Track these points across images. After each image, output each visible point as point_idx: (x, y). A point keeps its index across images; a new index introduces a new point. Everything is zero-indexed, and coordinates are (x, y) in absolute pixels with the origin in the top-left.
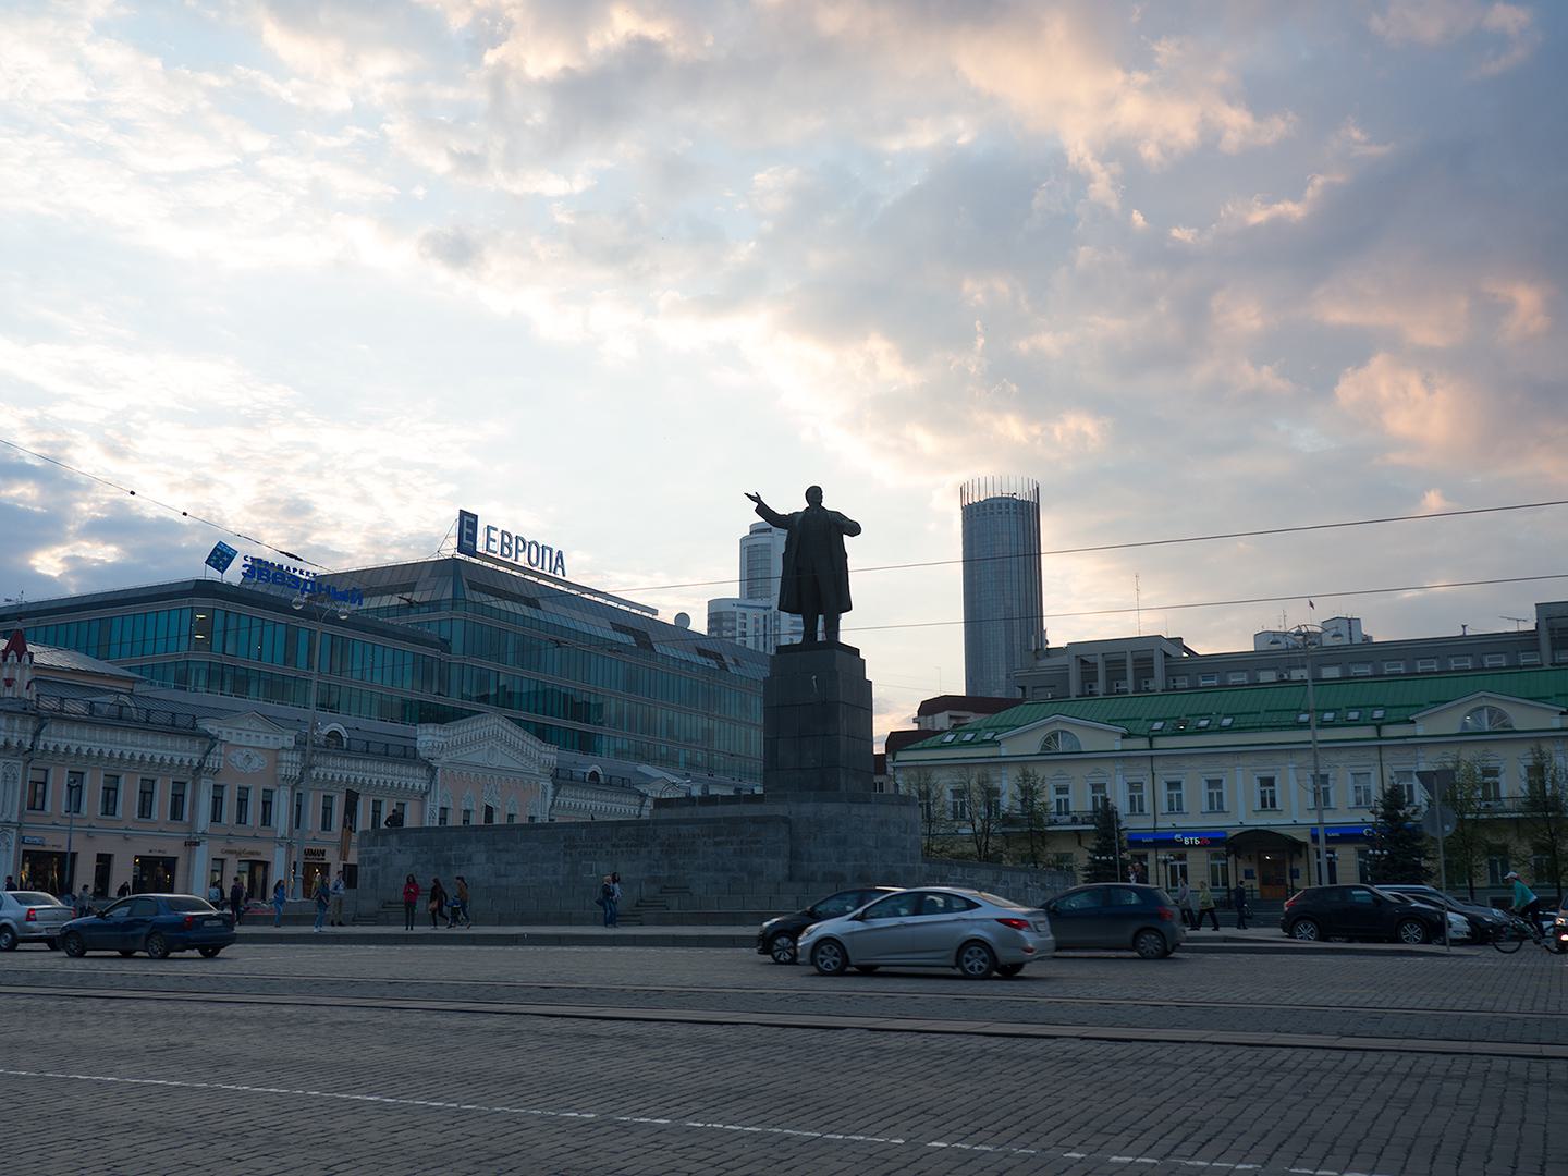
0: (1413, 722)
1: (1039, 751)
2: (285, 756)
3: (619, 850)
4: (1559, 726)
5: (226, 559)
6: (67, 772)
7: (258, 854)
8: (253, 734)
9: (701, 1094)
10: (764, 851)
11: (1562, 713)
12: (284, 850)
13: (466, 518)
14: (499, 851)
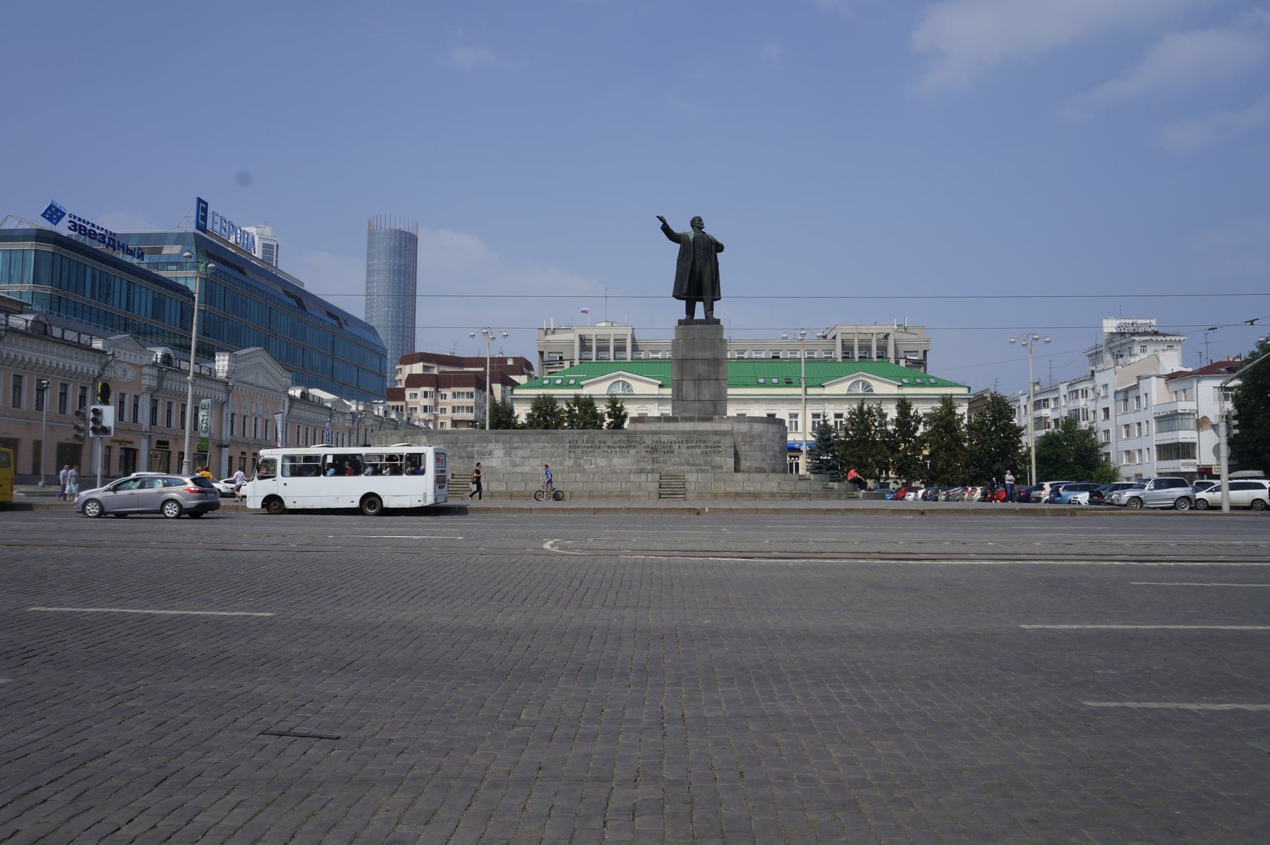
0: (823, 386)
2: (146, 370)
3: (613, 450)
4: (896, 393)
5: (59, 214)
6: (12, 376)
7: (132, 443)
8: (128, 353)
9: (405, 587)
10: (724, 453)
11: (899, 386)
12: (147, 440)
13: (201, 204)
14: (515, 448)
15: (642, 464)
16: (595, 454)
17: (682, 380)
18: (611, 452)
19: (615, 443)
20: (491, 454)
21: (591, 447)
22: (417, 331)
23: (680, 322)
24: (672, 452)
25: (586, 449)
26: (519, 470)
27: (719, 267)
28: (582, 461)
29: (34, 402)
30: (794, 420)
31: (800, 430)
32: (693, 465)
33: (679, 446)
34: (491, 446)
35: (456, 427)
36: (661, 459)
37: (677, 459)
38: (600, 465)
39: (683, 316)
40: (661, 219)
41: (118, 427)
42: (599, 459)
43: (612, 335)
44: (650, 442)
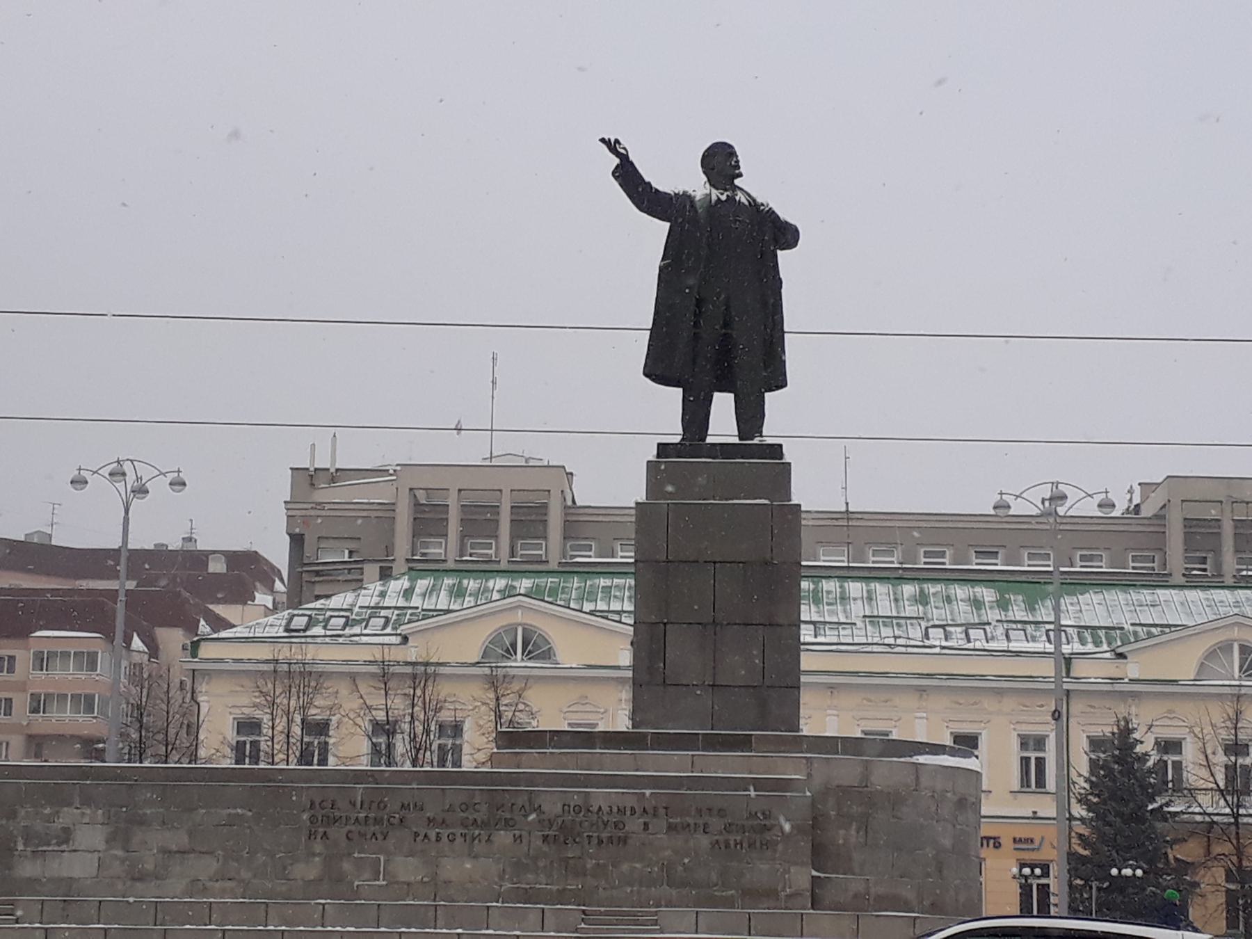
1: (1192, 678)
3: (445, 833)
15: (530, 876)
16: (391, 841)
18: (438, 839)
20: (66, 841)
25: (363, 829)
26: (148, 894)
28: (347, 866)
30: (1033, 755)
31: (1051, 784)
32: (684, 884)
33: (646, 824)
34: (67, 816)
35: (37, 756)
36: (590, 864)
39: (673, 431)
40: (612, 146)
42: (399, 859)
43: (506, 492)
44: (558, 809)
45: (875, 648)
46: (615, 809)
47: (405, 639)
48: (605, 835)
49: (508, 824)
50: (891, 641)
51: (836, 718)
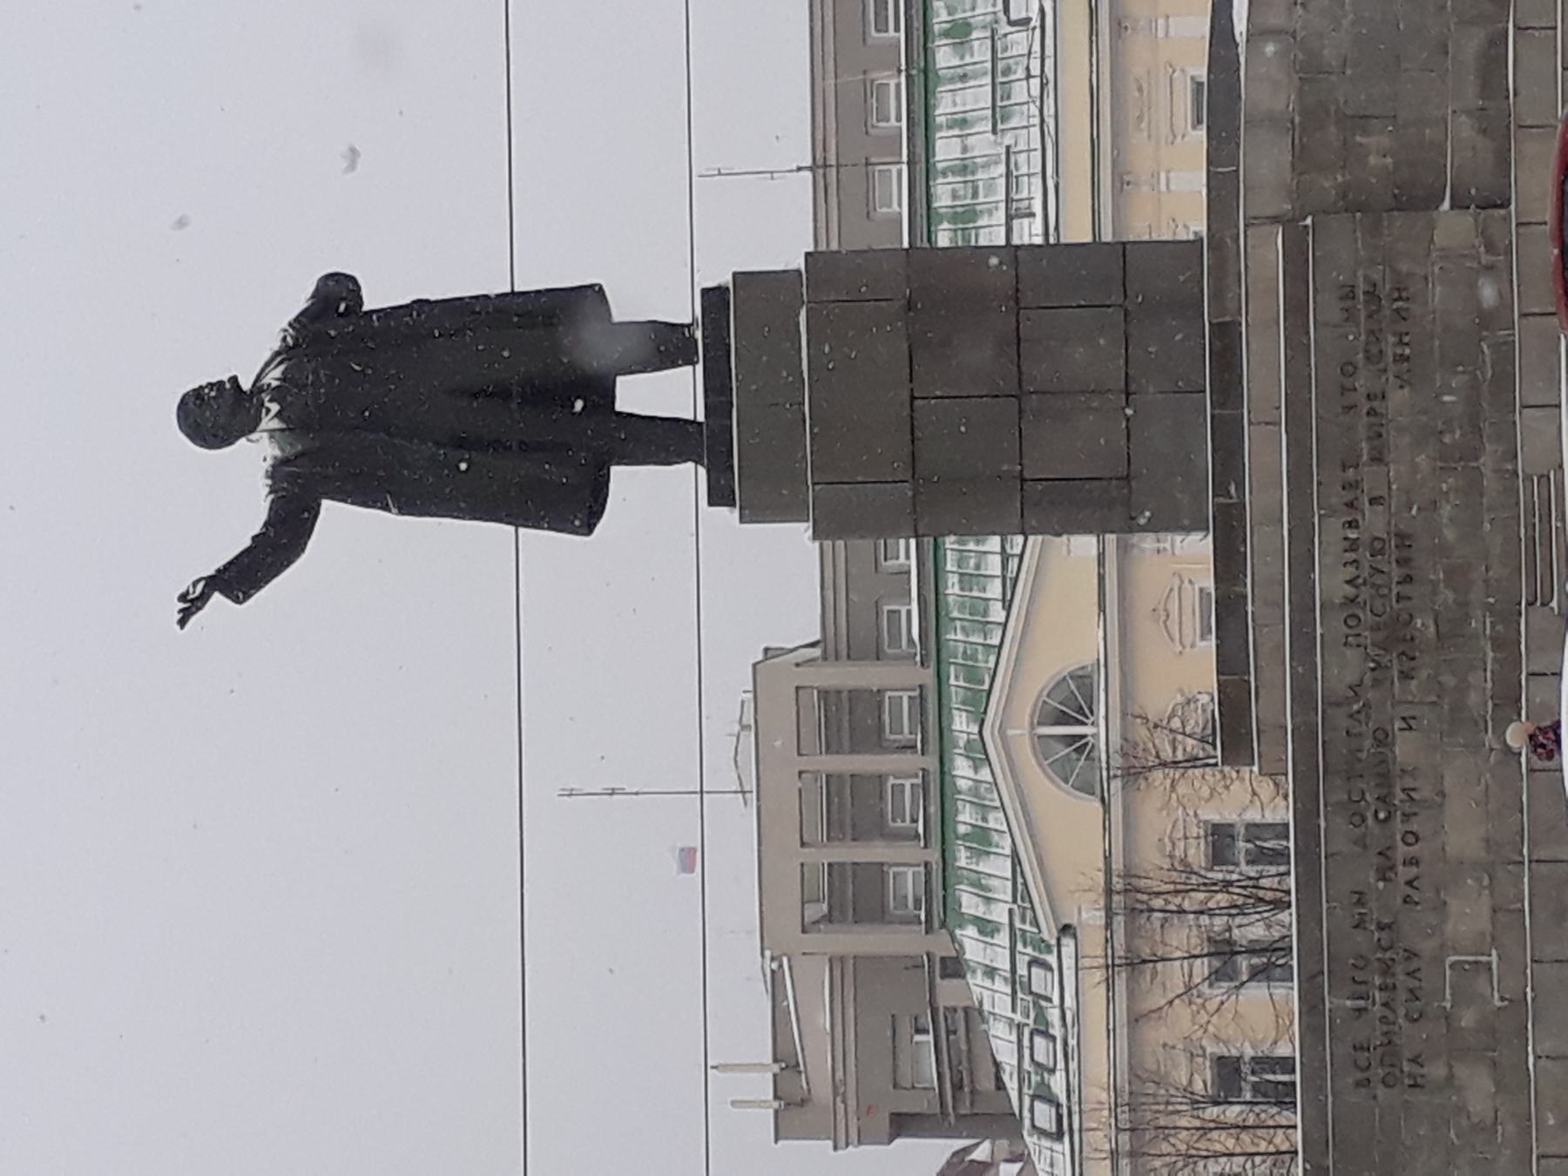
3: (1402, 851)
15: (1473, 698)
16: (1427, 947)
17: (1023, 480)
18: (1413, 861)
19: (1361, 842)
21: (1387, 969)
22: (527, 282)
23: (719, 495)
24: (1404, 540)
25: (1402, 995)
27: (433, 298)
28: (1468, 1019)
29: (1121, 848)
33: (1373, 501)
37: (1446, 510)
38: (1483, 922)
39: (688, 478)
40: (191, 605)
41: (1557, 774)
45: (1049, 110)
46: (1350, 556)
47: (1066, 929)
48: (1396, 573)
49: (1383, 739)
50: (1035, 83)
51: (1172, 175)
